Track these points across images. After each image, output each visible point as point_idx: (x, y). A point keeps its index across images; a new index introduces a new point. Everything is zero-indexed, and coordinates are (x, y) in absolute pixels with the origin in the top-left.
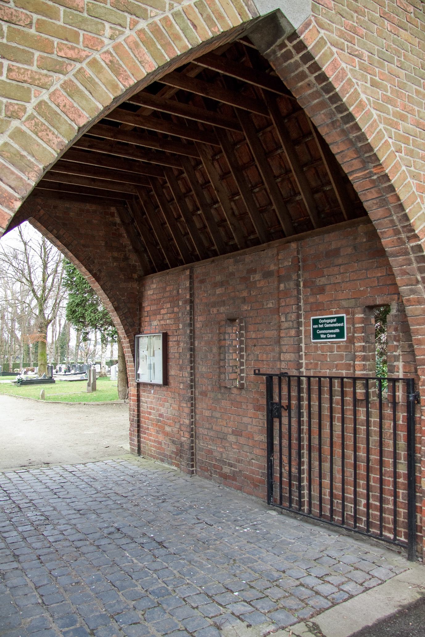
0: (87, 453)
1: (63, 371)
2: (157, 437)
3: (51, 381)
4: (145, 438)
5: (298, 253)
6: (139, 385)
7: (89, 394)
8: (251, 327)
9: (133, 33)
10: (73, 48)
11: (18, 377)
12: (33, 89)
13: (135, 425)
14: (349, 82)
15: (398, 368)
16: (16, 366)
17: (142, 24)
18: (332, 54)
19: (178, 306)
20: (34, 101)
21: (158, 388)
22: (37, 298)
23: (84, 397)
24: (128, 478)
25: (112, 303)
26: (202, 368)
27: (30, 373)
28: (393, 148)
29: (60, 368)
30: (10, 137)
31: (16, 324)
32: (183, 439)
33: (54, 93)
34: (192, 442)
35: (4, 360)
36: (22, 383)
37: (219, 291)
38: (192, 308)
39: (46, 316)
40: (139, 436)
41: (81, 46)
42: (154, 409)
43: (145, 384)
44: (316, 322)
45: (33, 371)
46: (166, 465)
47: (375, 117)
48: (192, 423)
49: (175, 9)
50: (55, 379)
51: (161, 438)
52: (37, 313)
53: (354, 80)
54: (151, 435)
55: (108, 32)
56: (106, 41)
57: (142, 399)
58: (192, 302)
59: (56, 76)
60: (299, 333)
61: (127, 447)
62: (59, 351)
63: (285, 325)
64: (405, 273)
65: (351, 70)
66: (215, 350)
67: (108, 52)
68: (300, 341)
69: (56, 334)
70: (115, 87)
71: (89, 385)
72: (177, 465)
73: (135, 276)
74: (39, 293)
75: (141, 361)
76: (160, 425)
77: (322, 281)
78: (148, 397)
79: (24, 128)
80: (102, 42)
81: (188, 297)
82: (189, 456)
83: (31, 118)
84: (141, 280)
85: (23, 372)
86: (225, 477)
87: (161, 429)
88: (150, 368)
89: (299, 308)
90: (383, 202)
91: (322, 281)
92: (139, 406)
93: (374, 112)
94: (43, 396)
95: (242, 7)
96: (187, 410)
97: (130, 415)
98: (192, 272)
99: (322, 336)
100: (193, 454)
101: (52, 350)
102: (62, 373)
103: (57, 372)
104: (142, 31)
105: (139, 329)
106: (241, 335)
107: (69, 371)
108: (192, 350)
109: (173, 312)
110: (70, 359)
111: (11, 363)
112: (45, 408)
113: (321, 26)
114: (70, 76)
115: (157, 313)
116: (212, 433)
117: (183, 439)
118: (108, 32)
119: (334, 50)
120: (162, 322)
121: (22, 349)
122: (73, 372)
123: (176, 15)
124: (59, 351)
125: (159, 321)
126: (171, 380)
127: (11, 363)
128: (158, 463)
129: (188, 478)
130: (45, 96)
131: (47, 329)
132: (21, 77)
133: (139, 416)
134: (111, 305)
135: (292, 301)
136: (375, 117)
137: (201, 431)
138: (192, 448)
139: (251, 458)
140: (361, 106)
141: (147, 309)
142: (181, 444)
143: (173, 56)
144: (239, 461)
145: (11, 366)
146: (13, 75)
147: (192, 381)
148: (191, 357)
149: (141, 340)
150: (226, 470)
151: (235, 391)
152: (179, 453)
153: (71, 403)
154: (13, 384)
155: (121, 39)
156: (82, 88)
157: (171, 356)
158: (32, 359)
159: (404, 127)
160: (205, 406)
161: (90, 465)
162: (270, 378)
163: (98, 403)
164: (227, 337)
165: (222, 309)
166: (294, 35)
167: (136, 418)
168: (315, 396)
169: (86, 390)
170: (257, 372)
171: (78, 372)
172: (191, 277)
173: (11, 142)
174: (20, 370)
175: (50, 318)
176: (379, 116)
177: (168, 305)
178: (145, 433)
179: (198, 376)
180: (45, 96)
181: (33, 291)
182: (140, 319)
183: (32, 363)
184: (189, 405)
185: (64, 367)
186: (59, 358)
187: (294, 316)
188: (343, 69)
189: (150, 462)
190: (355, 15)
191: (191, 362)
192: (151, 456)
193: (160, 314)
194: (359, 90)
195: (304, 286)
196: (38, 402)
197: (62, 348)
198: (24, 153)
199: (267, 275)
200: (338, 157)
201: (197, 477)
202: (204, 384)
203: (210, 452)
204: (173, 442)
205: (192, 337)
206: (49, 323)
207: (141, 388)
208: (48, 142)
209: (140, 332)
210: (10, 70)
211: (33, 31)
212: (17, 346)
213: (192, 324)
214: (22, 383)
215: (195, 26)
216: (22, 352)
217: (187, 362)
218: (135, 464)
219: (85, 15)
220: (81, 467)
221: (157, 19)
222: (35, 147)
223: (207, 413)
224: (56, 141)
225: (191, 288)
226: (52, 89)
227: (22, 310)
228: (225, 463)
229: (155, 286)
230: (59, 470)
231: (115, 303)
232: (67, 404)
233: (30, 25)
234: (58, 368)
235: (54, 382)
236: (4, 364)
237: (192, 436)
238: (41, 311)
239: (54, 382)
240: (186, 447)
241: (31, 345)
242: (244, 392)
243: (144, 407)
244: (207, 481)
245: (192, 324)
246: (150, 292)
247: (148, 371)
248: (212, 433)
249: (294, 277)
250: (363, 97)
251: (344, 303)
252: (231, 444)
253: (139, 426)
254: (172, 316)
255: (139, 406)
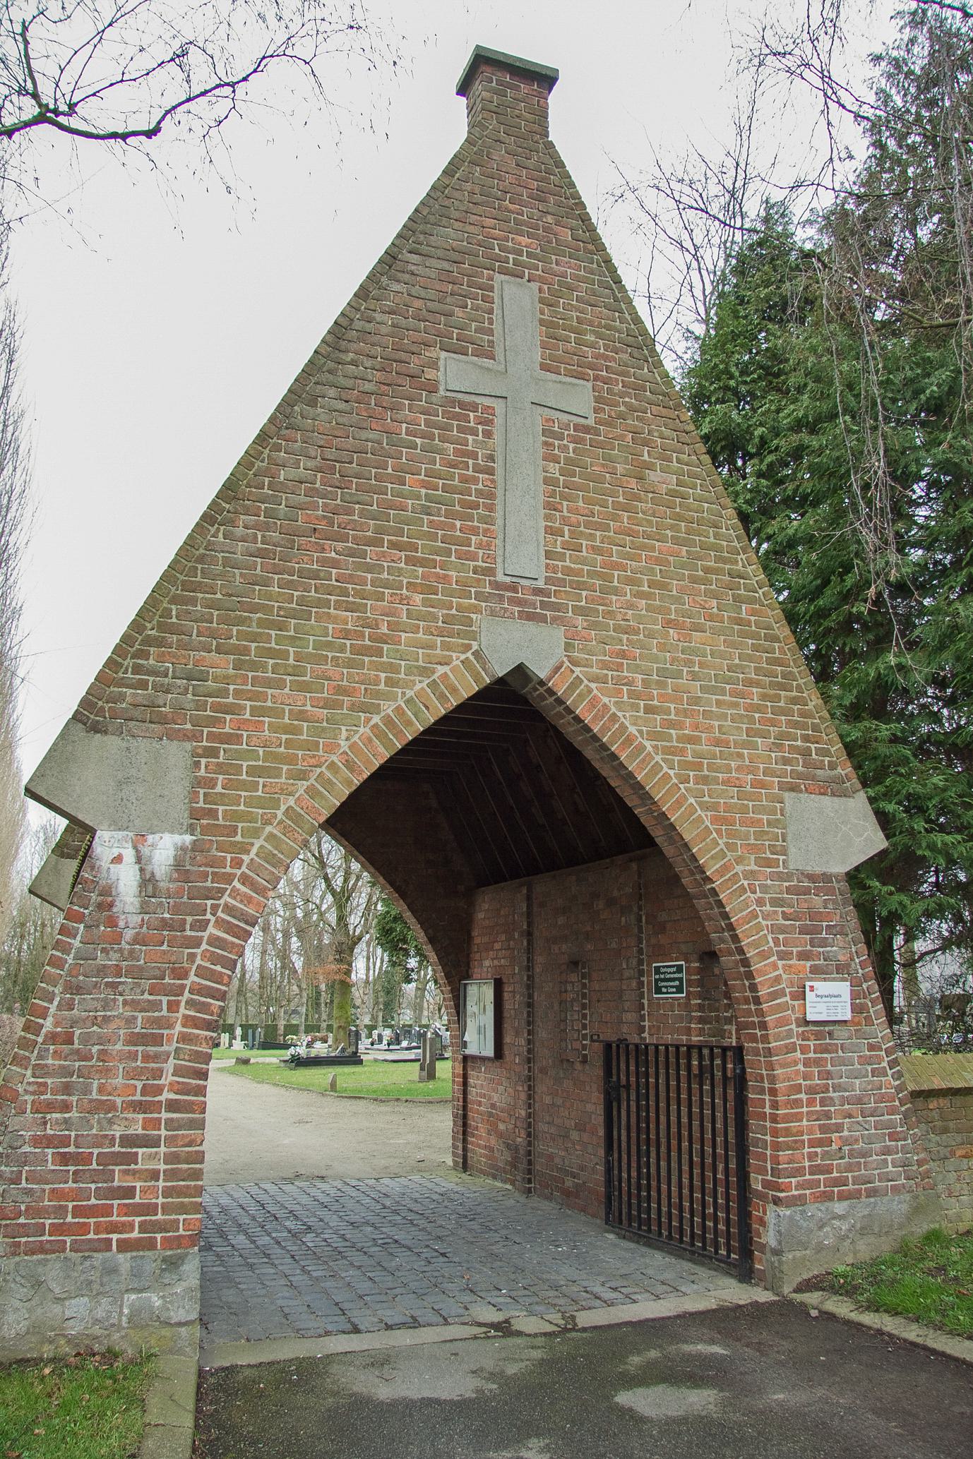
3: (354, 1059)
4: (472, 1143)
5: (639, 877)
9: (367, 730)
10: (314, 756)
14: (614, 718)
17: (376, 719)
18: (590, 691)
20: (283, 808)
22: (334, 893)
26: (542, 1034)
27: (318, 1045)
28: (675, 781)
31: (294, 939)
34: (530, 1144)
37: (561, 920)
39: (351, 928)
40: (465, 1141)
41: (321, 753)
42: (484, 1096)
43: (474, 1058)
44: (657, 968)
46: (499, 1184)
47: (649, 748)
48: (529, 1116)
51: (493, 1141)
53: (620, 714)
54: (480, 1137)
55: (344, 734)
56: (342, 743)
57: (471, 1081)
58: (529, 934)
60: (641, 984)
63: (627, 974)
64: (710, 919)
65: (616, 703)
66: (556, 1007)
69: (374, 964)
70: (350, 782)
71: (422, 1069)
72: (513, 1183)
74: (338, 883)
75: (468, 1021)
77: (663, 916)
83: (281, 822)
86: (567, 1193)
87: (493, 1130)
90: (672, 842)
91: (663, 916)
92: (465, 1093)
93: (647, 744)
94: (333, 1085)
95: (479, 673)
96: (523, 1096)
98: (530, 890)
99: (664, 990)
102: (384, 1046)
104: (376, 725)
106: (584, 986)
110: (406, 1017)
111: (281, 1024)
112: (332, 1105)
114: (312, 781)
115: (488, 947)
117: (519, 1140)
118: (344, 734)
119: (593, 685)
121: (305, 994)
122: (405, 1044)
123: (409, 702)
127: (281, 1024)
129: (523, 1199)
131: (351, 955)
133: (465, 1108)
136: (649, 748)
137: (542, 1127)
138: (529, 1153)
139: (583, 1156)
140: (629, 740)
141: (477, 940)
143: (404, 743)
144: (582, 1168)
147: (529, 1051)
148: (529, 1016)
149: (469, 988)
150: (569, 1183)
151: (578, 1066)
154: (282, 1065)
155: (356, 738)
157: (506, 1014)
158: (324, 1017)
161: (386, 1181)
162: (608, 1046)
164: (569, 988)
166: (542, 683)
169: (416, 1077)
171: (414, 1044)
172: (529, 898)
173: (266, 844)
176: (655, 747)
181: (326, 879)
183: (324, 1025)
185: (387, 1033)
186: (381, 1014)
187: (634, 962)
189: (477, 1180)
191: (529, 1023)
194: (627, 724)
197: (388, 993)
199: (611, 902)
203: (551, 1157)
204: (508, 1146)
205: (530, 987)
206: (355, 944)
209: (468, 977)
210: (264, 786)
211: (282, 749)
212: (295, 988)
215: (427, 708)
217: (523, 1023)
221: (389, 711)
223: (548, 1100)
224: (300, 838)
225: (529, 914)
227: (307, 914)
228: (568, 1173)
229: (486, 906)
230: (338, 1184)
233: (280, 746)
235: (360, 1062)
237: (529, 1135)
238: (341, 918)
239: (360, 1062)
241: (323, 987)
243: (473, 1092)
246: (481, 915)
249: (635, 909)
250: (632, 730)
251: (683, 948)
253: (465, 1125)
255: (465, 1093)
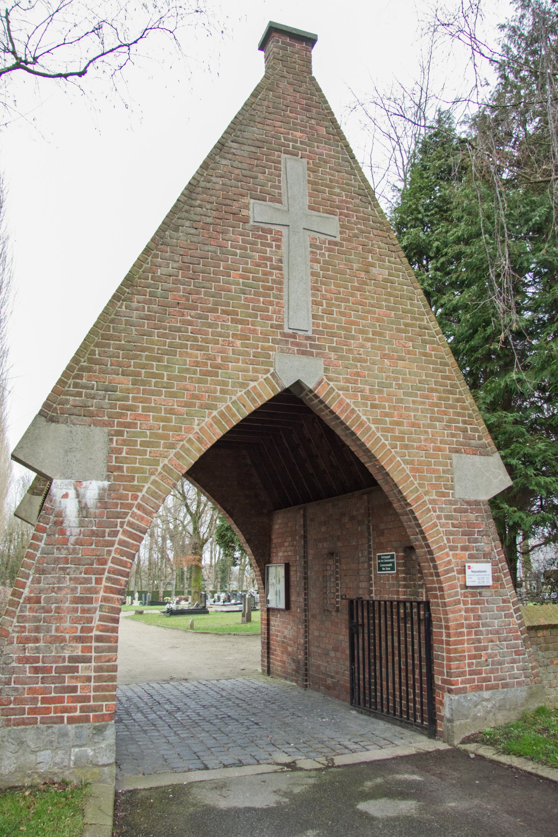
0: (223, 673)
1: (222, 600)
2: (282, 657)
3: (204, 611)
4: (273, 659)
6: (269, 610)
7: (243, 625)
8: (343, 561)
9: (210, 419)
11: (168, 606)
12: (161, 459)
13: (266, 647)
14: (353, 411)
15: (422, 594)
16: (168, 593)
17: (215, 413)
18: (339, 396)
19: (296, 540)
20: (161, 465)
21: (283, 613)
22: (191, 514)
23: (236, 628)
24: (252, 690)
25: (245, 536)
26: (313, 595)
28: (389, 447)
29: (219, 598)
30: (151, 484)
31: (168, 541)
32: (300, 657)
33: (170, 459)
35: (153, 587)
36: (172, 613)
37: (323, 529)
38: (305, 542)
39: (201, 534)
40: (268, 658)
41: (183, 433)
43: (274, 609)
45: (187, 601)
46: (288, 682)
48: (306, 642)
49: (233, 400)
50: (209, 609)
51: (285, 658)
52: (191, 532)
54: (278, 656)
55: (196, 422)
56: (195, 427)
57: (272, 623)
58: (305, 537)
59: (171, 450)
60: (370, 566)
61: (260, 670)
62: (219, 576)
63: (362, 560)
65: (354, 402)
66: (321, 579)
67: (197, 433)
68: (370, 572)
70: (200, 450)
71: (243, 616)
72: (296, 682)
73: (265, 511)
74: (193, 508)
76: (284, 645)
77: (382, 526)
78: (276, 621)
79: (157, 479)
80: (193, 428)
81: (302, 533)
82: (304, 673)
83: (160, 473)
84: (270, 515)
85: (175, 602)
86: (328, 688)
88: (276, 595)
89: (369, 547)
91: (382, 526)
94: (192, 626)
95: (274, 386)
96: (302, 631)
97: (262, 638)
99: (383, 569)
100: (306, 670)
101: (210, 575)
102: (221, 603)
103: (214, 602)
105: (269, 559)
106: (337, 567)
107: (230, 601)
108: (306, 578)
109: (293, 546)
110: (234, 586)
111: (161, 590)
112: (191, 638)
113: (330, 379)
114: (178, 449)
115: (281, 545)
116: (319, 651)
117: (300, 657)
118: (196, 422)
119: (341, 392)
120: (286, 554)
121: (175, 573)
122: (233, 601)
123: (234, 403)
124: (219, 576)
125: (284, 552)
126: (292, 606)
127: (161, 590)
128: (283, 681)
129: (302, 691)
130: (166, 461)
132: (155, 455)
133: (268, 638)
134: (243, 538)
135: (365, 541)
137: (313, 649)
138: (306, 664)
140: (362, 424)
141: (275, 541)
142: (299, 662)
144: (337, 673)
145: (161, 594)
146: (152, 454)
147: (305, 605)
148: (305, 584)
150: (329, 681)
151: (334, 613)
152: (297, 671)
153: (221, 633)
154: (162, 614)
155: (203, 424)
156: (183, 454)
157: (292, 584)
158: (186, 586)
159: (399, 430)
160: (315, 627)
162: (351, 602)
163: (248, 633)
165: (325, 545)
166: (311, 391)
167: (266, 641)
168: (383, 616)
170: (344, 597)
171: (239, 602)
172: (304, 516)
174: (172, 600)
175: (205, 537)
177: (290, 539)
178: (273, 654)
179: (310, 601)
180: (166, 461)
181: (187, 506)
182: (270, 550)
183: (186, 591)
184: (304, 627)
185: (223, 596)
186: (219, 584)
187: (366, 553)
188: (348, 404)
189: (276, 680)
190: (359, 364)
192: (278, 675)
193: (283, 546)
194: (361, 414)
195: (373, 530)
196: (186, 631)
197: (223, 572)
198: (157, 491)
200: (355, 453)
201: (310, 690)
202: (314, 608)
203: (318, 667)
204: (294, 660)
205: (306, 567)
206: (204, 544)
207: (271, 613)
208: (168, 484)
209: (270, 562)
210: (150, 452)
211: (160, 431)
212: (169, 569)
213: (305, 557)
214: (172, 613)
215: (244, 406)
216: (175, 577)
217: (302, 589)
218: (262, 681)
219: (185, 416)
220: (215, 682)
221: (223, 408)
222: (162, 487)
223: (316, 633)
225: (305, 526)
226: (169, 458)
227: (176, 527)
228: (328, 676)
230: (195, 683)
231: (247, 536)
232: (216, 634)
234: (216, 597)
235: (207, 612)
236: (153, 592)
237: (306, 654)
238: (196, 529)
239: (207, 612)
240: (302, 664)
241: (185, 569)
242: (339, 614)
243: (273, 629)
244: (316, 693)
245: (305, 557)
246: (276, 527)
247: (274, 597)
248: (319, 651)
249: (366, 522)
251: (395, 544)
252: (332, 659)
254: (292, 548)
